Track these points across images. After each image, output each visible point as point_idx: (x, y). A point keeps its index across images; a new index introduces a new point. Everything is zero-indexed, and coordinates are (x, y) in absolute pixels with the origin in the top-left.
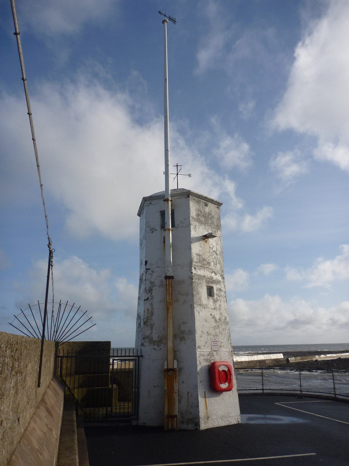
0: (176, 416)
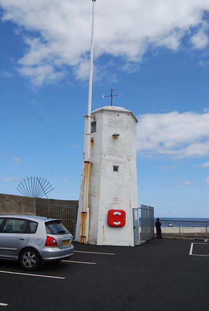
0: (86, 237)
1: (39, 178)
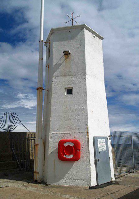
1: (11, 113)
